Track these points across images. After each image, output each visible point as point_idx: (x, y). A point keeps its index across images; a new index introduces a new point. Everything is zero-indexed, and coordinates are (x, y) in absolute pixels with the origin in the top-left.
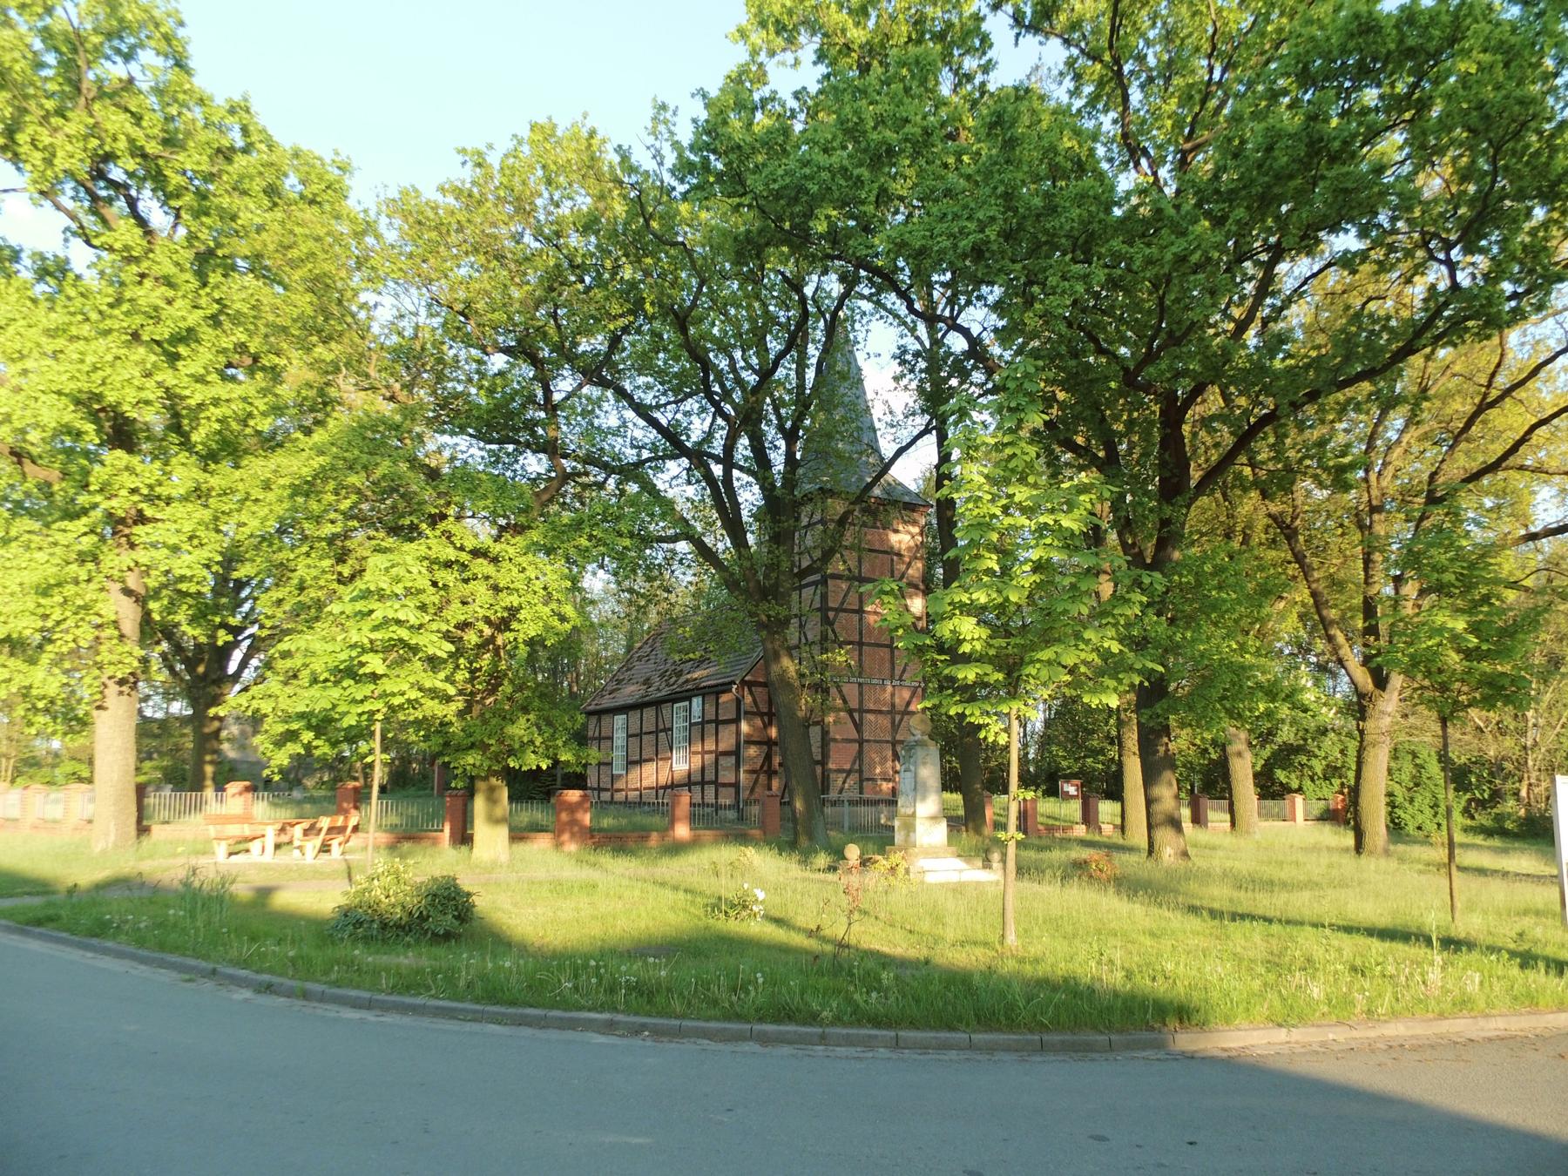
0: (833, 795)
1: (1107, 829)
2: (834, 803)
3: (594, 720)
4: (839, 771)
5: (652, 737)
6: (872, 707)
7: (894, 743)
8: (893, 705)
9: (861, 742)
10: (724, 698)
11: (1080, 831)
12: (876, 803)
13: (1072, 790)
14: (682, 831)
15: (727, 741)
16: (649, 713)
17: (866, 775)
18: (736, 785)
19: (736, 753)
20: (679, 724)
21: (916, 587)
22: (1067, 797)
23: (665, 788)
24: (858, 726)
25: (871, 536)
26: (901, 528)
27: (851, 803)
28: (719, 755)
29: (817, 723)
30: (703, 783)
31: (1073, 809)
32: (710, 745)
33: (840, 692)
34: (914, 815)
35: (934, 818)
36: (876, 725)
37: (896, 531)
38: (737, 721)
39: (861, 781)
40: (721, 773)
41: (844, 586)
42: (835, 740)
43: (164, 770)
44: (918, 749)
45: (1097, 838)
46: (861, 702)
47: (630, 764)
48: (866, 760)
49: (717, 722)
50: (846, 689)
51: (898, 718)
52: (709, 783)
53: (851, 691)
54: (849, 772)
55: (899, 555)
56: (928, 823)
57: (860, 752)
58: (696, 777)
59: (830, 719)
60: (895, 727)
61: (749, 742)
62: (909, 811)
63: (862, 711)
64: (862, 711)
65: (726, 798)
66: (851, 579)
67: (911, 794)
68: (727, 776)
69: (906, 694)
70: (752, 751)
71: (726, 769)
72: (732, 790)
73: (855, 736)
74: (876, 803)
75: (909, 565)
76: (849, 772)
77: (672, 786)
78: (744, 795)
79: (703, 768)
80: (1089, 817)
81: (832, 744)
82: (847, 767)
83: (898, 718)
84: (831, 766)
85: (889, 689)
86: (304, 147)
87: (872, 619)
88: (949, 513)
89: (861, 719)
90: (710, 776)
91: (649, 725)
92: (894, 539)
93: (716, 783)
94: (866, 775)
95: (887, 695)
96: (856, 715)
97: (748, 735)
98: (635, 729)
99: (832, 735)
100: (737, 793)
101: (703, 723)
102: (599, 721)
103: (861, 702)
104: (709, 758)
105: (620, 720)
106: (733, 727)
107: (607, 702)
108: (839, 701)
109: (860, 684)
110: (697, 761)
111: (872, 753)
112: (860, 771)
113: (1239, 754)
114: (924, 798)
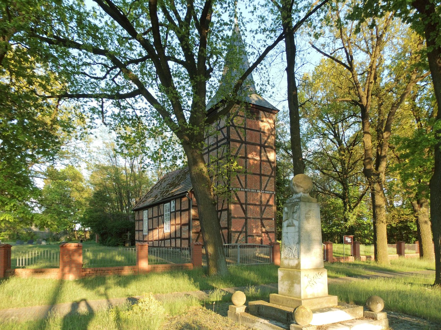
0: (233, 243)
1: (363, 258)
2: (234, 247)
3: (137, 213)
4: (236, 232)
5: (156, 219)
6: (251, 202)
7: (262, 219)
8: (261, 202)
9: (246, 218)
10: (184, 199)
11: (351, 259)
12: (254, 247)
13: (349, 240)
14: (144, 265)
15: (185, 220)
16: (155, 208)
17: (249, 234)
18: (189, 239)
19: (188, 224)
20: (166, 213)
21: (272, 148)
22: (347, 243)
23: (162, 240)
24: (245, 211)
25: (250, 123)
26: (264, 119)
27: (241, 247)
28: (183, 225)
29: (225, 210)
30: (176, 238)
31: (347, 248)
32: (178, 221)
33: (236, 194)
34: (298, 267)
35: (317, 269)
36: (254, 211)
37: (262, 121)
38: (189, 210)
39: (246, 236)
40: (183, 233)
41: (238, 145)
42: (234, 218)
43: (10, 236)
44: (302, 204)
45: (357, 262)
46: (246, 200)
47: (150, 230)
48: (249, 227)
49: (181, 211)
50: (239, 194)
51: (263, 208)
52: (178, 238)
53: (242, 195)
54: (241, 232)
55: (264, 132)
56: (312, 274)
57: (246, 223)
58: (173, 236)
59: (232, 207)
60: (262, 212)
61: (194, 219)
62: (293, 263)
63: (246, 204)
64: (246, 204)
65: (185, 244)
66: (241, 142)
67: (295, 247)
68: (185, 235)
69: (268, 196)
70: (197, 223)
71: (184, 232)
72: (187, 241)
73: (244, 216)
74: (254, 247)
75: (268, 138)
76: (241, 232)
77: (164, 239)
78: (193, 242)
79: (176, 232)
80: (355, 253)
81: (233, 220)
82: (240, 230)
83: (263, 208)
84: (233, 229)
85: (259, 194)
86: (320, 324)
87: (251, 161)
88: (294, 93)
89: (246, 208)
90: (178, 235)
91: (155, 215)
92: (261, 125)
93: (180, 238)
94: (249, 234)
95: (259, 197)
96: (244, 206)
97: (194, 216)
98: (150, 216)
99: (232, 215)
100: (189, 242)
101: (175, 211)
102: (139, 213)
103: (246, 200)
104: (178, 227)
105: (145, 213)
106: (187, 212)
107: (141, 205)
108: (236, 199)
109: (246, 192)
110: (173, 228)
111: (251, 223)
112: (246, 232)
113: (426, 222)
114: (309, 249)
